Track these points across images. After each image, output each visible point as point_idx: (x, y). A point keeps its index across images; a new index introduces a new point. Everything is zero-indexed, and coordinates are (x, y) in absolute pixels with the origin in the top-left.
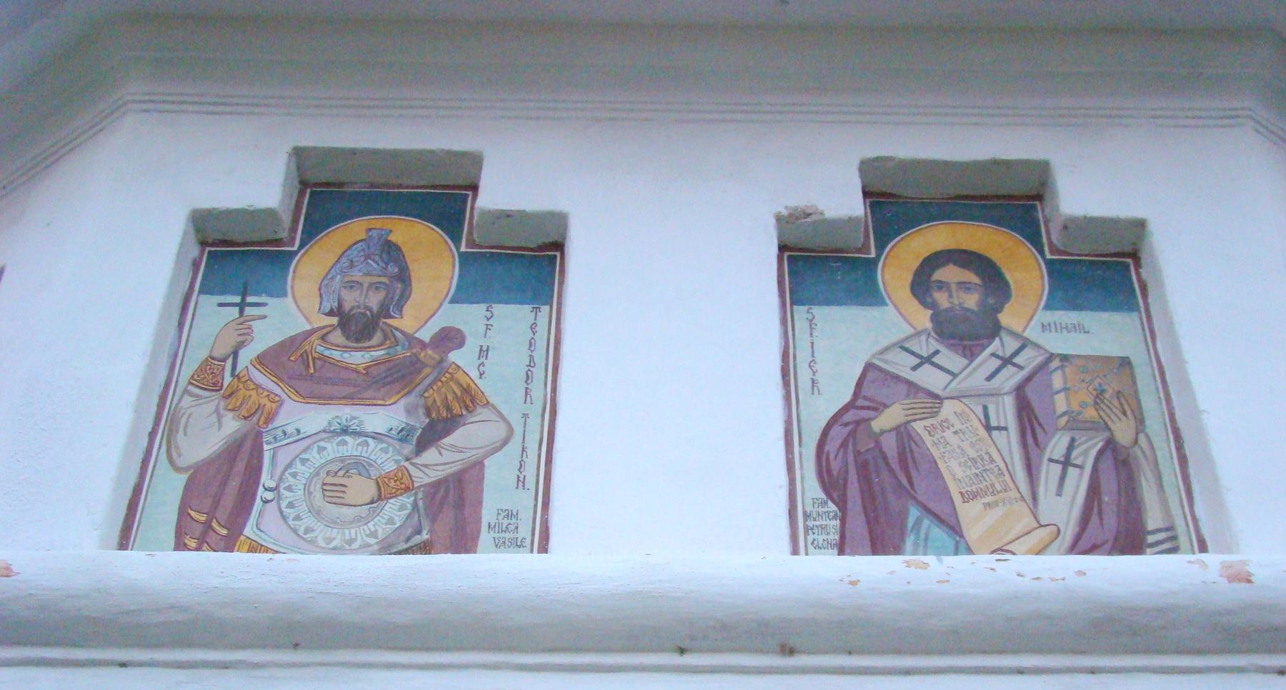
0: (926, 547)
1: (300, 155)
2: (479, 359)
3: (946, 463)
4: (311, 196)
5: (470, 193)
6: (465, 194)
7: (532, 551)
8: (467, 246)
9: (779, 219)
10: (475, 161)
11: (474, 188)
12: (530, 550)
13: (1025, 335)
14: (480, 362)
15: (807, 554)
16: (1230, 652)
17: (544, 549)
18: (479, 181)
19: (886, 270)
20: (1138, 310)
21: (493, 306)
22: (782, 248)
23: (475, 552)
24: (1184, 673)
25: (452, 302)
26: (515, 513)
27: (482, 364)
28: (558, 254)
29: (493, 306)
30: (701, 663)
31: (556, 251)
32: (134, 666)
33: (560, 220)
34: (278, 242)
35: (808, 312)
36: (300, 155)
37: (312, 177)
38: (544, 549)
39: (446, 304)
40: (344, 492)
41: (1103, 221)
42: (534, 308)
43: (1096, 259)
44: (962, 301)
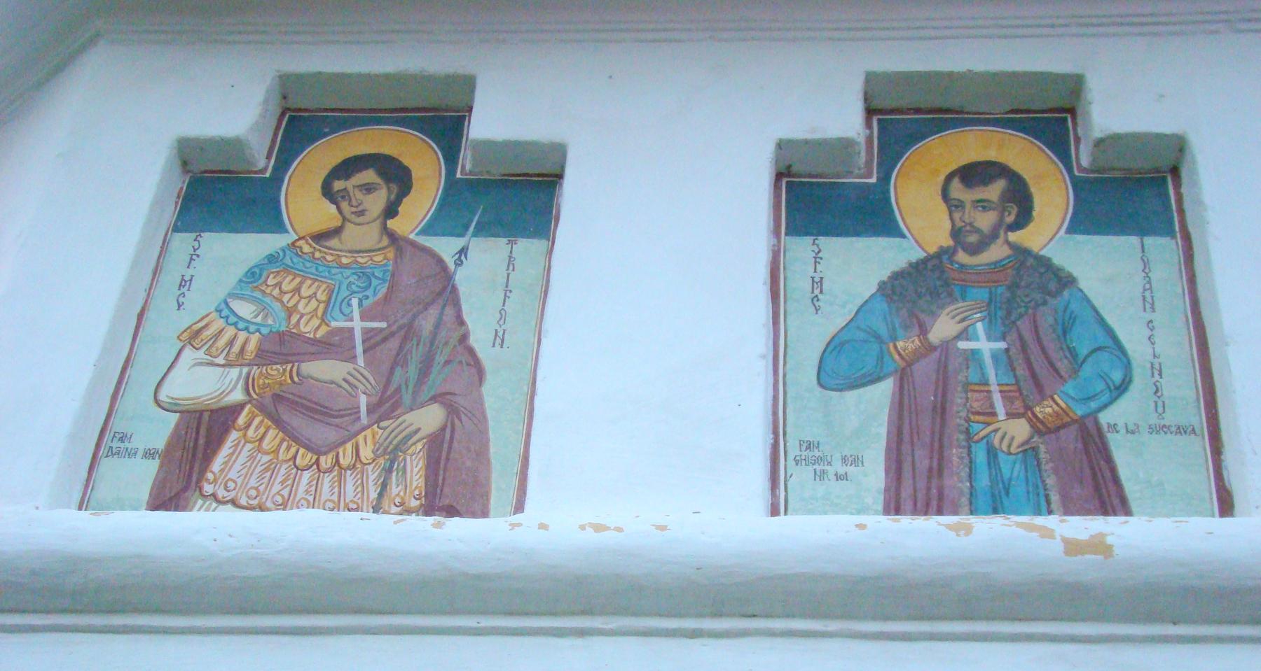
0: (1003, 508)
1: (871, 80)
2: (179, 289)
3: (801, 451)
5: (467, 114)
6: (463, 115)
10: (468, 84)
14: (181, 292)
15: (786, 513)
19: (899, 179)
21: (202, 234)
22: (782, 174)
23: (485, 514)
24: (56, 631)
26: (129, 436)
27: (183, 295)
29: (202, 234)
31: (878, 179)
32: (532, 614)
33: (1178, 146)
35: (814, 244)
36: (871, 80)
37: (877, 104)
41: (1035, 74)
42: (509, 240)
44: (972, 220)
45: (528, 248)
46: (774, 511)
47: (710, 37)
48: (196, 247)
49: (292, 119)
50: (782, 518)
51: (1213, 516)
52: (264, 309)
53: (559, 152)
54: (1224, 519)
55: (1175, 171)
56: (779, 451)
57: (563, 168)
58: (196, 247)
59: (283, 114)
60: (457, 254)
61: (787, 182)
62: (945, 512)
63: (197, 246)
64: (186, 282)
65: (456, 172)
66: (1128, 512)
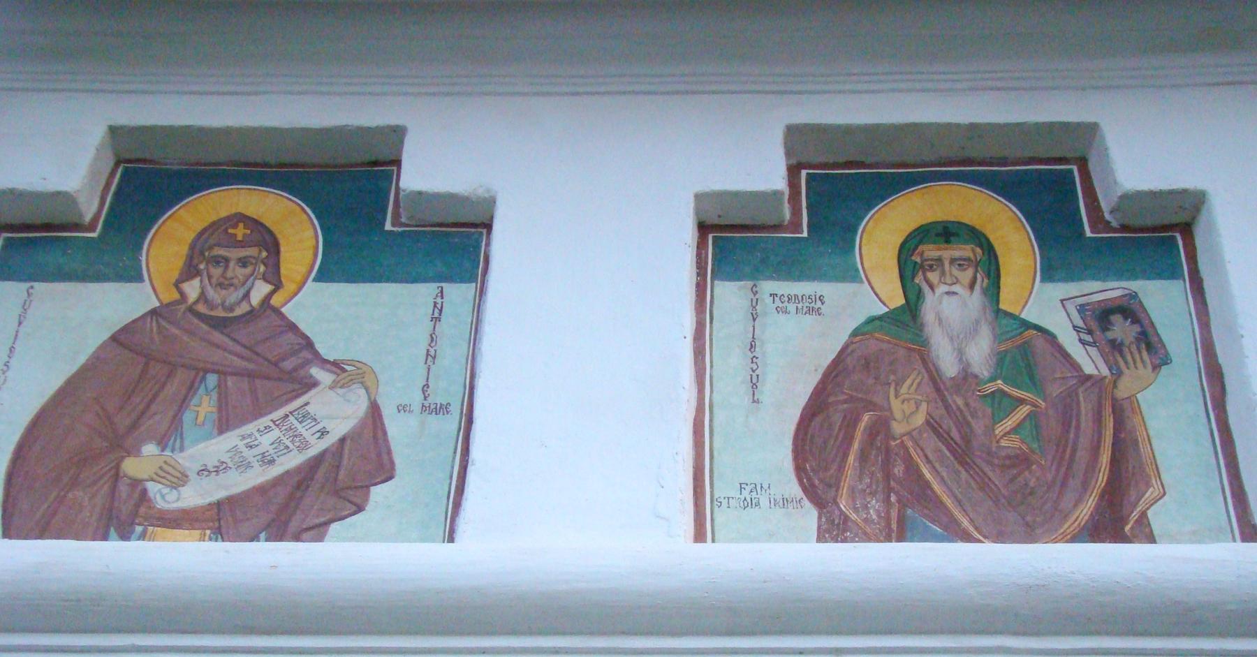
1: (114, 132)
4: (123, 176)
7: (444, 542)
8: (393, 225)
9: (699, 197)
10: (397, 134)
11: (397, 163)
12: (442, 539)
13: (1023, 316)
15: (713, 541)
16: (1178, 635)
17: (451, 539)
18: (401, 156)
20: (861, 282)
22: (704, 228)
25: (317, 279)
28: (485, 231)
30: (580, 645)
34: (76, 227)
38: (451, 539)
39: (310, 283)
40: (161, 468)
43: (416, 229)
45: (459, 294)
46: (699, 536)
47: (812, 81)
48: (754, 369)
49: (126, 170)
50: (708, 545)
51: (1234, 540)
52: (834, 510)
53: (489, 204)
54: (1244, 544)
55: (1187, 229)
56: (704, 481)
57: (492, 218)
58: (754, 369)
59: (117, 164)
60: (1084, 347)
61: (714, 237)
62: (909, 534)
63: (755, 367)
64: (426, 407)
65: (385, 220)
66: (1151, 539)
